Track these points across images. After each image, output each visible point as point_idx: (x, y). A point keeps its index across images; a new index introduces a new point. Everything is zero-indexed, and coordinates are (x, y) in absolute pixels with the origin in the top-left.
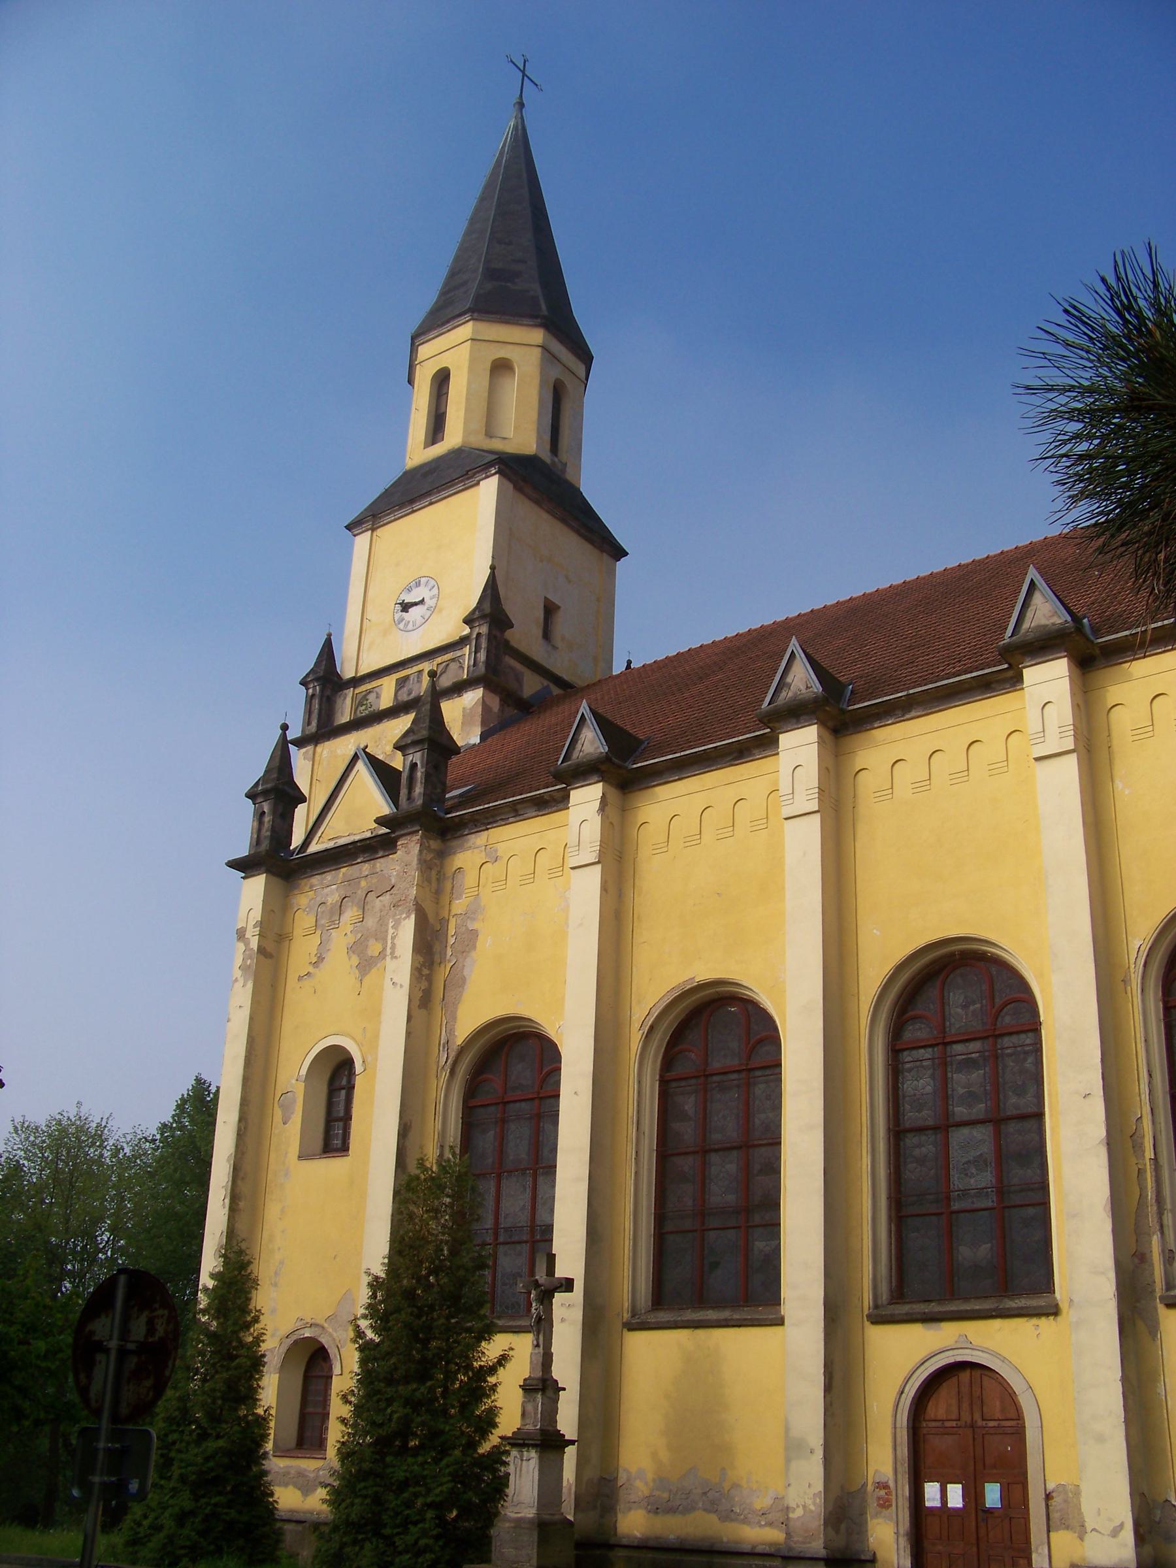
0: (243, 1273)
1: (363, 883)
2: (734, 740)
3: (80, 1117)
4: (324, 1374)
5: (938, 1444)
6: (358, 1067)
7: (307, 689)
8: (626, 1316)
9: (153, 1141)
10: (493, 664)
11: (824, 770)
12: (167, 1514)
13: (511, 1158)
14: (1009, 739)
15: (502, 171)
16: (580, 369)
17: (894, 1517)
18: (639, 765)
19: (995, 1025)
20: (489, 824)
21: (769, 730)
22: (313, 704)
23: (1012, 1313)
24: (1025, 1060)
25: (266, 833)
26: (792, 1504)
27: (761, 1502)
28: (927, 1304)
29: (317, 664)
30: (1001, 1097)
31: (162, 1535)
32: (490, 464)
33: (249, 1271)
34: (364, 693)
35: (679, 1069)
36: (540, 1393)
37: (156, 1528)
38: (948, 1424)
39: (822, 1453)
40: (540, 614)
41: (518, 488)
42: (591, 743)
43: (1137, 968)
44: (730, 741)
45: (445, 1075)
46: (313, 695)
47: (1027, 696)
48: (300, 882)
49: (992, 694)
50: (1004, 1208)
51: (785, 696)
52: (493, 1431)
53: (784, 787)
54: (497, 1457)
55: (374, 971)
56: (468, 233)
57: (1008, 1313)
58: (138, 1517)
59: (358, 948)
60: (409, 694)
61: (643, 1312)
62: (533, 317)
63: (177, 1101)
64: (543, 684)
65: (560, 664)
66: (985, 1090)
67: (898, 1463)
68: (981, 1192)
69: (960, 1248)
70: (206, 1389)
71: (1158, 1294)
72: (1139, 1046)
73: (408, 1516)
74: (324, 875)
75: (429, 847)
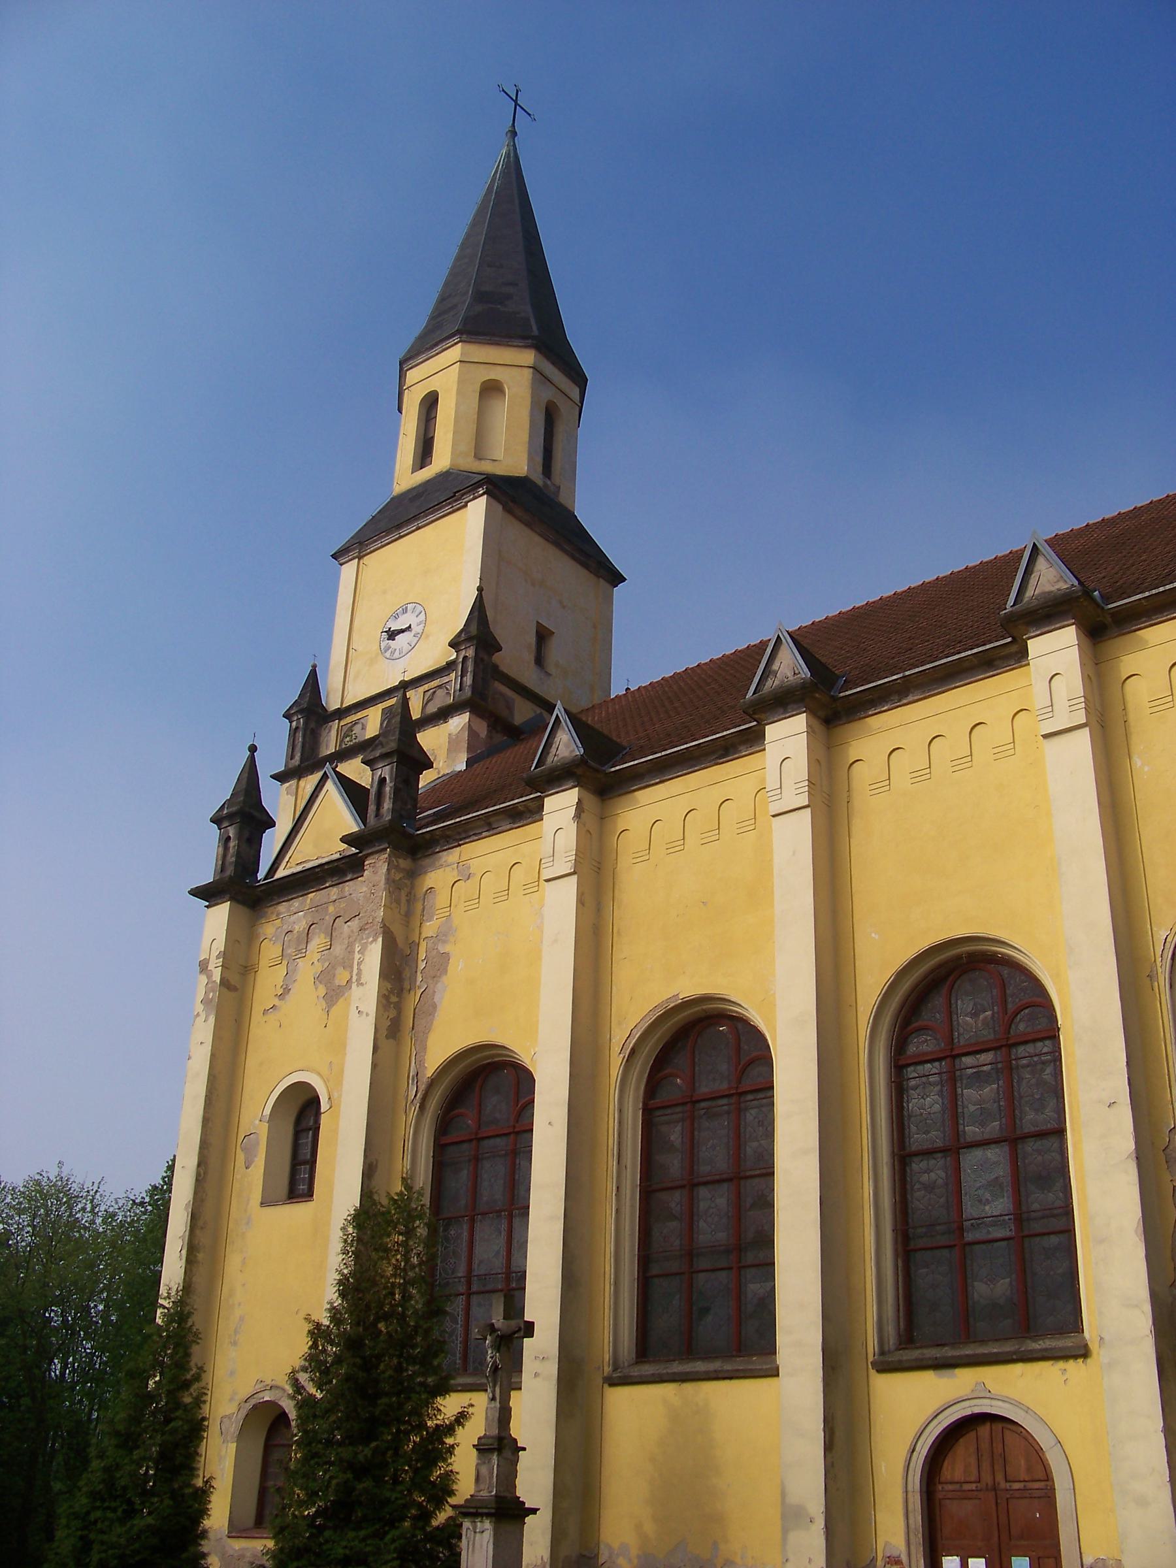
0: (183, 1325)
1: (331, 909)
2: (718, 736)
3: (62, 1178)
5: (956, 1510)
6: (324, 1106)
7: (291, 722)
8: (607, 1370)
9: (142, 1204)
11: (814, 762)
13: (485, 1199)
14: (1015, 720)
16: (575, 393)
18: (618, 768)
19: (1009, 1033)
21: (755, 723)
22: (297, 738)
23: (1035, 1355)
24: (1043, 1070)
25: (231, 859)
28: (939, 1349)
30: (1017, 1112)
32: (478, 485)
33: (190, 1324)
34: (350, 724)
35: (664, 1096)
36: (496, 1454)
38: (966, 1487)
39: (823, 1523)
40: (532, 639)
41: (507, 510)
43: (1164, 961)
44: (714, 737)
45: (413, 1111)
46: (297, 728)
48: (266, 910)
49: (995, 672)
51: (771, 684)
53: (772, 782)
54: (452, 1532)
55: (341, 1000)
57: (1030, 1356)
59: (324, 977)
61: (626, 1364)
62: (524, 338)
63: (168, 1162)
64: (535, 712)
66: (1000, 1106)
67: (911, 1535)
68: (997, 1220)
69: (976, 1283)
70: (135, 1457)
75: (398, 866)
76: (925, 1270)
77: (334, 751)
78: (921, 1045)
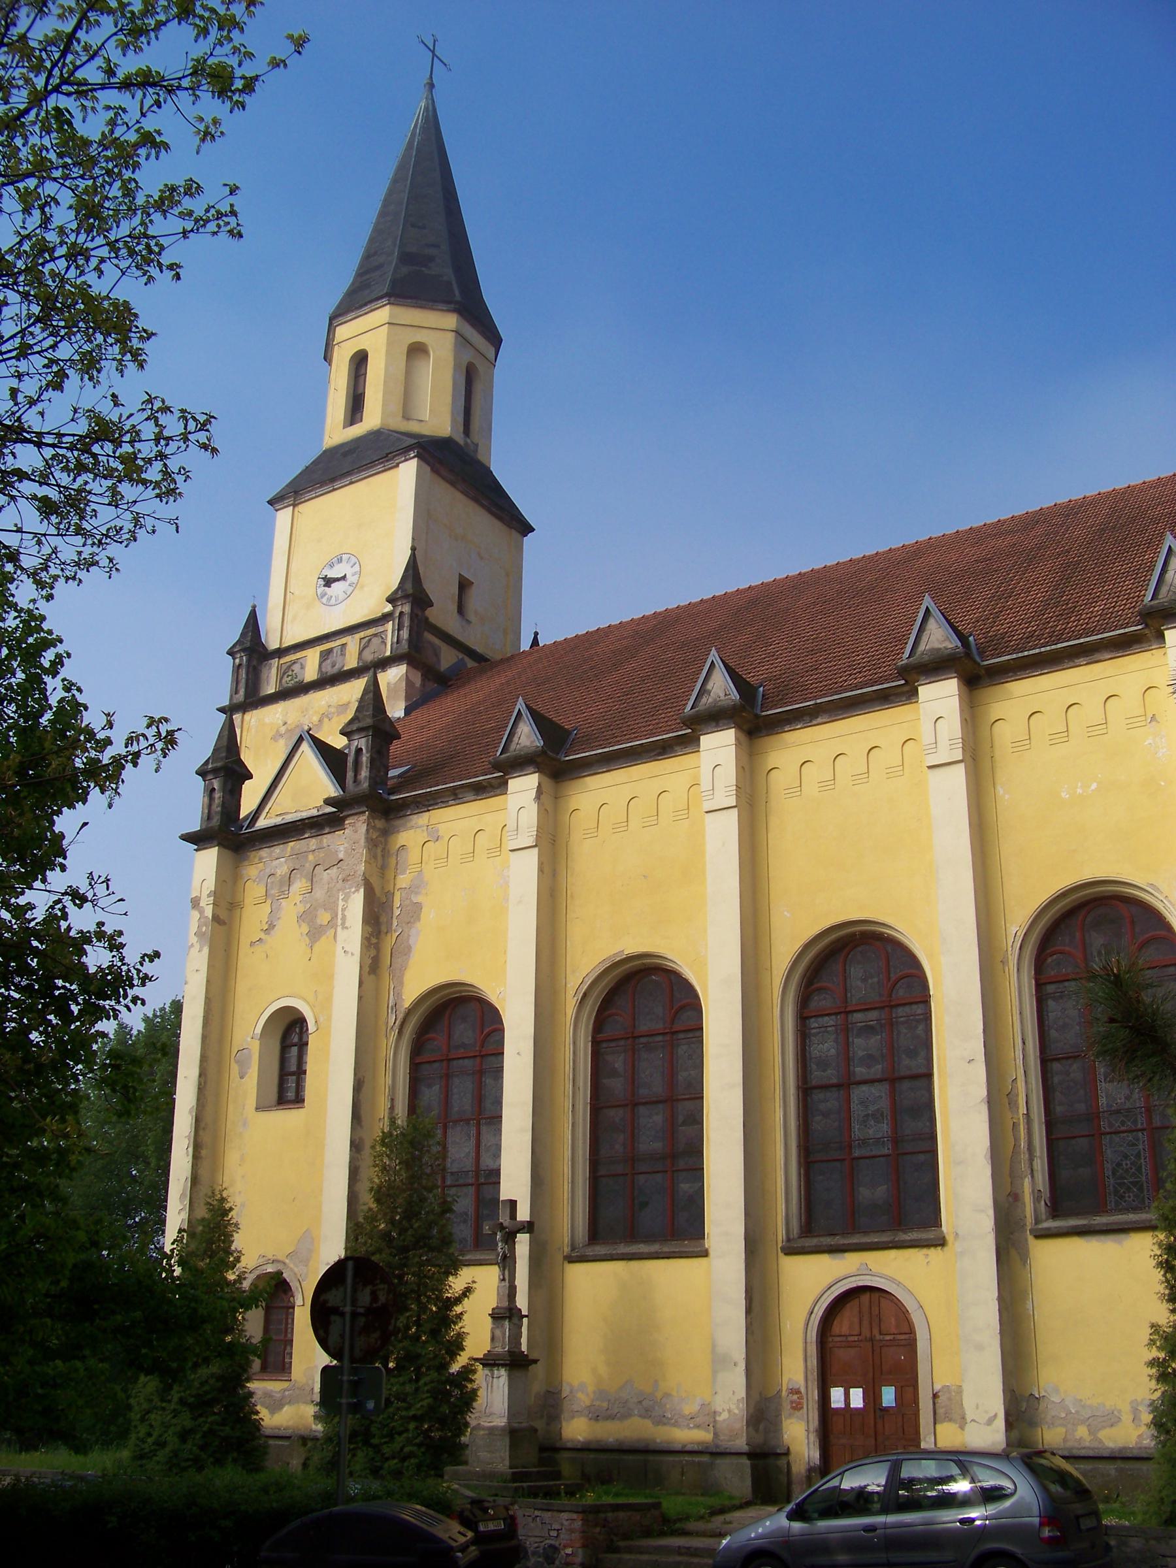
1: (311, 857)
4: (285, 1305)
5: (843, 1355)
6: (311, 1027)
7: (234, 659)
8: (567, 1250)
10: (415, 641)
12: (170, 1432)
15: (414, 153)
16: (490, 352)
17: (805, 1416)
18: (571, 757)
19: (891, 996)
20: (430, 805)
21: (690, 731)
22: (240, 673)
25: (217, 808)
26: (719, 1409)
27: (690, 1408)
28: (833, 1237)
29: (243, 635)
30: (896, 1059)
31: (167, 1450)
33: (230, 1217)
34: (288, 664)
37: (161, 1444)
40: (455, 590)
41: (435, 470)
42: (527, 736)
46: (240, 665)
47: (921, 711)
48: (248, 854)
49: (890, 706)
50: (898, 1155)
51: (706, 701)
52: (462, 1353)
53: (705, 784)
55: (323, 939)
56: (382, 214)
58: (141, 1435)
60: (333, 666)
61: (581, 1245)
62: (449, 302)
64: (458, 657)
65: (473, 638)
67: (808, 1372)
69: (861, 1189)
71: (1029, 1227)
72: (1015, 1018)
73: (394, 1428)
74: (272, 849)
76: (821, 1177)
77: (273, 691)
78: (819, 1002)
